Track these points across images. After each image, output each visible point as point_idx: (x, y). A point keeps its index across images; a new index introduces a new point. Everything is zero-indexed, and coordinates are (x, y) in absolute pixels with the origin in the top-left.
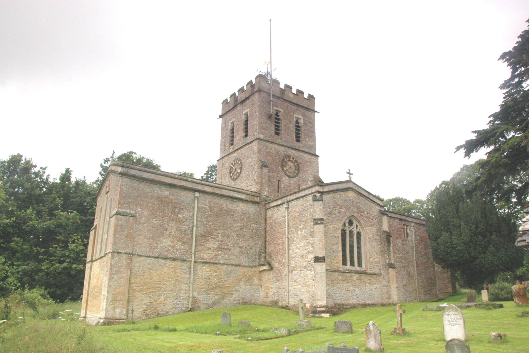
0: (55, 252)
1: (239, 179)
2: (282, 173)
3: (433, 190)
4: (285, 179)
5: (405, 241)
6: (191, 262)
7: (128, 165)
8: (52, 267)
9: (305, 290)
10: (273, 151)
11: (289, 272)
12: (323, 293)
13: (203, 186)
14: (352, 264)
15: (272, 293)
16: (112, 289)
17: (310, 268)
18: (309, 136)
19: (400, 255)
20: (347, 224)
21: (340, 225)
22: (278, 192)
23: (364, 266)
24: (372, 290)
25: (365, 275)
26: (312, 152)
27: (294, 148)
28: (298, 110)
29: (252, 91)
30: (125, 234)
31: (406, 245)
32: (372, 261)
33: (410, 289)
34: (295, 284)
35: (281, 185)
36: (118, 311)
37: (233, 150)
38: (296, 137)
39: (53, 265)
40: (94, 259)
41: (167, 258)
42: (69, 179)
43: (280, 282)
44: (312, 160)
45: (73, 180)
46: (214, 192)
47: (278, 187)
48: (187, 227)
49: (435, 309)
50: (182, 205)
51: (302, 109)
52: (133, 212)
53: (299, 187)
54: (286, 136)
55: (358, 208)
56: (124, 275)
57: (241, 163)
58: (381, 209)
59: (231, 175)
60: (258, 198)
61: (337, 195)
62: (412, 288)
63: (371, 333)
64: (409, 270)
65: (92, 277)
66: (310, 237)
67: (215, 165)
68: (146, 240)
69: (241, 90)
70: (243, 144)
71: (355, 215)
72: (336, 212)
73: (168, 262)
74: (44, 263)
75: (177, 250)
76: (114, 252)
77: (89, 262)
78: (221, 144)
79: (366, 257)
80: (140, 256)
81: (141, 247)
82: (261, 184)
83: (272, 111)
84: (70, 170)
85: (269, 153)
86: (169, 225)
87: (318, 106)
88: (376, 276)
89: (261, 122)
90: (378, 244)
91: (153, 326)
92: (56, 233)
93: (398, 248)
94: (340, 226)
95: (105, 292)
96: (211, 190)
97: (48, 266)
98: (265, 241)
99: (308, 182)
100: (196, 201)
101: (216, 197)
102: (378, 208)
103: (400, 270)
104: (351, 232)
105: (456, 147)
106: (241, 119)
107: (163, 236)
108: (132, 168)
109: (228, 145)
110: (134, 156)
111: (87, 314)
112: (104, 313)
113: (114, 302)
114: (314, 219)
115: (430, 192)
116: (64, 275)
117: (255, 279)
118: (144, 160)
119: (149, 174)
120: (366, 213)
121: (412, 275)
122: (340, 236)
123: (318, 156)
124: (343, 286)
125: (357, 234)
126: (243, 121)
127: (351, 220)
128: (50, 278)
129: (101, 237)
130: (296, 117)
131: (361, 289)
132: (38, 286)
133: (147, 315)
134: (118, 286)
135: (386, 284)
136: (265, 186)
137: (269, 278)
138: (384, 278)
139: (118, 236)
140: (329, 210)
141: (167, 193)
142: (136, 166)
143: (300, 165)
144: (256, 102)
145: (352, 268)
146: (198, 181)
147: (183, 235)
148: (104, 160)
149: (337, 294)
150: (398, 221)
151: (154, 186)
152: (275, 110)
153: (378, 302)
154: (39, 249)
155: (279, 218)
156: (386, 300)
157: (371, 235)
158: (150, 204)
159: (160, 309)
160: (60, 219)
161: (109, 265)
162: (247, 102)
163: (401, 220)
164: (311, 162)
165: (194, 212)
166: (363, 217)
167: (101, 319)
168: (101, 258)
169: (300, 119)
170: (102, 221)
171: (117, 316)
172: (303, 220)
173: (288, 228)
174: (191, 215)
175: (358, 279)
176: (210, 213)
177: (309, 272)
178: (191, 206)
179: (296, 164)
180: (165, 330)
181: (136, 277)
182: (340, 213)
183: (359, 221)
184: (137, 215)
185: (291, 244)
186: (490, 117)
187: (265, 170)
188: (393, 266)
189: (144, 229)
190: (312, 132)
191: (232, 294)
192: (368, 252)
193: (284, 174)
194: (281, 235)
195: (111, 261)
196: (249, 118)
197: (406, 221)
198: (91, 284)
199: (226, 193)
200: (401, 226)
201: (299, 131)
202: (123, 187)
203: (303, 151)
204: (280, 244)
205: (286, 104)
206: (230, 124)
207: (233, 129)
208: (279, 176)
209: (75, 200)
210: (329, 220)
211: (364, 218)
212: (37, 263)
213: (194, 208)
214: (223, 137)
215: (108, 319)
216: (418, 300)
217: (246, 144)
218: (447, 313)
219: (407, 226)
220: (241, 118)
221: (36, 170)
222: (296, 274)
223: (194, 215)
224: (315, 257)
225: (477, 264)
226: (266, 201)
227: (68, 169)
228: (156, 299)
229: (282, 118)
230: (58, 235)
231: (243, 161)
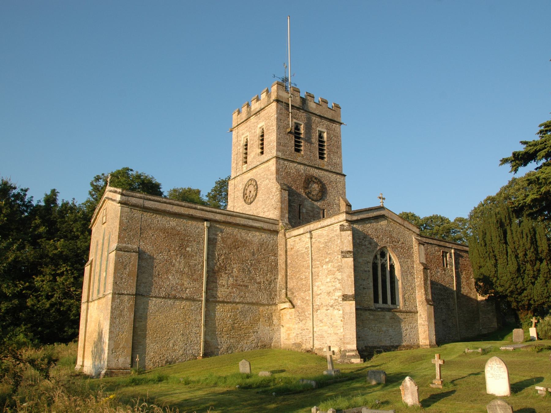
3: (476, 206)
6: (202, 301)
9: (332, 332)
11: (313, 311)
12: (353, 335)
14: (385, 301)
15: (295, 334)
17: (337, 307)
20: (379, 256)
21: (371, 258)
26: (338, 171)
34: (321, 325)
35: (302, 210)
37: (247, 169)
38: (320, 153)
43: (304, 322)
45: (59, 203)
46: (226, 220)
48: (196, 262)
63: (408, 389)
65: (88, 320)
66: (338, 272)
67: (224, 180)
94: (371, 258)
98: (286, 275)
103: (439, 304)
105: (502, 159)
106: (256, 134)
108: (133, 197)
109: (241, 163)
110: (130, 173)
114: (342, 252)
115: (473, 209)
117: (275, 318)
119: (152, 202)
122: (371, 270)
123: (345, 176)
124: (374, 327)
126: (258, 136)
129: (98, 275)
130: (319, 131)
131: (394, 329)
135: (423, 323)
136: (285, 212)
137: (291, 317)
140: (358, 241)
144: (273, 115)
145: (385, 306)
149: (368, 335)
152: (295, 123)
155: (300, 249)
156: (423, 341)
161: (110, 308)
162: (263, 113)
163: (439, 246)
170: (99, 256)
172: (329, 252)
173: (312, 262)
175: (392, 318)
177: (336, 312)
181: (141, 320)
185: (316, 279)
186: (540, 126)
189: (148, 266)
190: (338, 148)
191: (249, 337)
194: (304, 269)
199: (240, 221)
201: (322, 147)
203: (327, 171)
204: (303, 279)
207: (246, 145)
208: (301, 199)
218: (490, 365)
221: (15, 192)
222: (320, 314)
224: (343, 296)
227: (54, 190)
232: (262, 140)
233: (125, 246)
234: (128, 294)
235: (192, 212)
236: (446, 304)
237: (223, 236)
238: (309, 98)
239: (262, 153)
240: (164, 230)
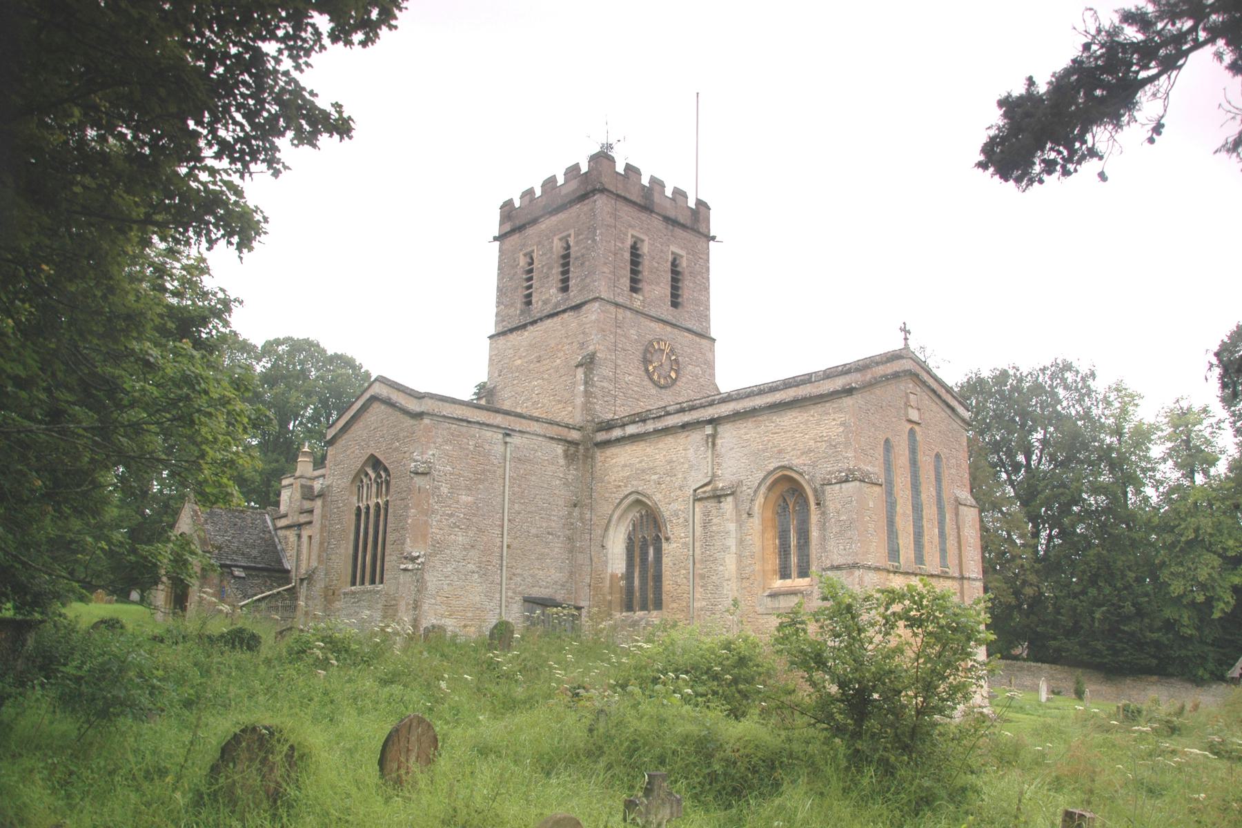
130: (673, 253)
146: (459, 412)
169: (682, 257)
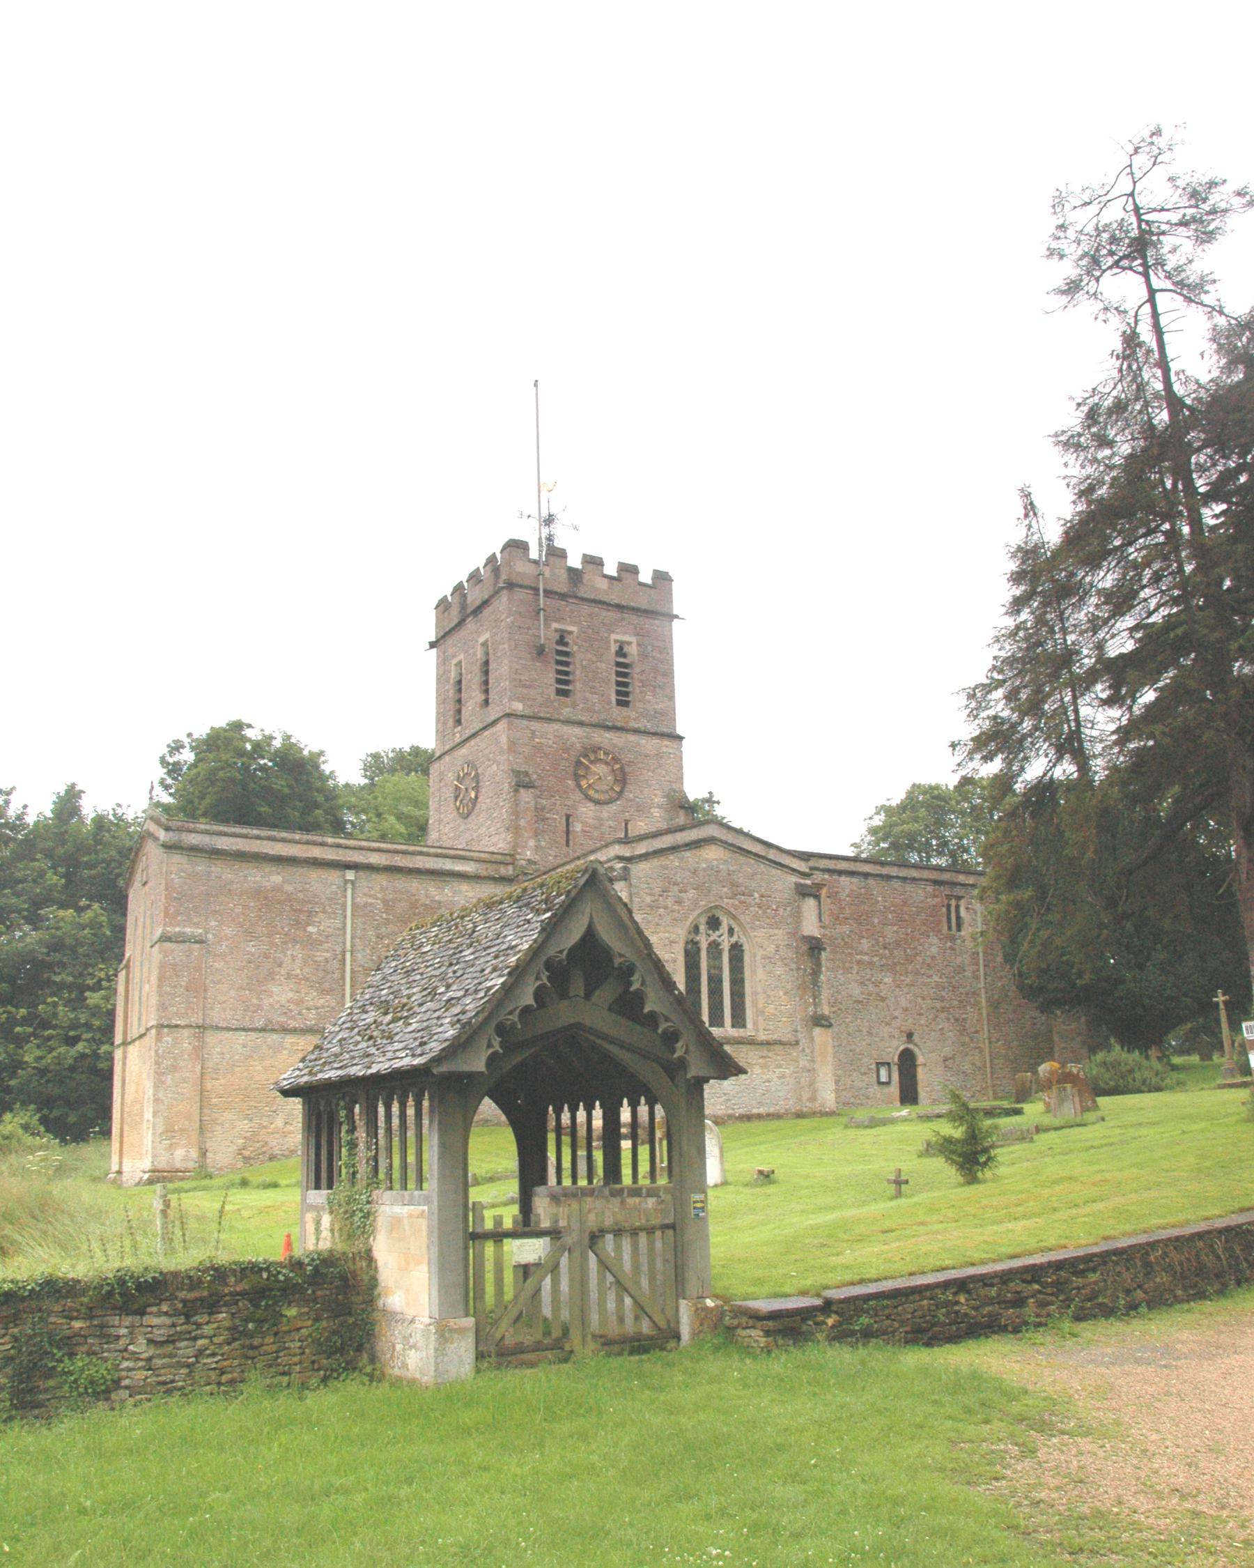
0: (55, 1015)
1: (473, 816)
2: (578, 796)
4: (587, 811)
5: (953, 939)
7: (180, 823)
8: (50, 1056)
10: (551, 742)
13: (364, 852)
16: (161, 1107)
18: (655, 687)
19: (936, 978)
20: (702, 928)
21: (680, 932)
22: (568, 845)
23: (749, 1024)
24: (769, 1082)
25: (748, 1046)
26: (666, 730)
27: (610, 724)
28: (623, 619)
29: (495, 585)
30: (183, 984)
31: (954, 949)
32: (772, 1011)
33: (967, 1067)
36: (179, 1153)
39: (51, 1049)
40: (129, 1040)
41: (286, 1030)
42: (75, 811)
44: (664, 749)
47: (568, 832)
49: (866, 1123)
50: (316, 903)
51: (634, 617)
52: (200, 931)
53: (626, 824)
54: (588, 694)
55: (733, 885)
56: (188, 1074)
57: (477, 775)
58: (802, 881)
59: (458, 803)
60: (510, 868)
61: (673, 860)
62: (973, 1064)
64: (964, 1016)
65: (127, 1079)
68: (233, 993)
69: (475, 577)
70: (481, 726)
71: (725, 902)
72: (670, 902)
73: (289, 1039)
74: (30, 1045)
75: (308, 1009)
76: (162, 1026)
77: (119, 1046)
78: (438, 721)
79: (755, 1003)
80: (223, 1029)
81: (224, 1010)
82: (515, 829)
83: (546, 634)
84: (78, 788)
85: (538, 749)
86: (285, 955)
87: (680, 602)
88: (782, 1047)
89: (517, 670)
90: (792, 970)
91: (237, 1178)
92: (49, 966)
93: (928, 960)
95: (148, 1115)
96: (387, 859)
97: (38, 1053)
99: (652, 810)
100: (349, 892)
101: (399, 876)
102: (794, 879)
104: (714, 947)
107: (273, 979)
109: (451, 723)
110: (248, 733)
111: (124, 1164)
112: (150, 1160)
113: (169, 1134)
116: (82, 1073)
118: (277, 743)
119: (232, 840)
120: (756, 895)
121: (973, 1030)
123: (681, 738)
125: (730, 951)
126: (478, 664)
127: (714, 916)
128: (48, 1081)
130: (616, 641)
132: (18, 1105)
133: (247, 1159)
134: (175, 1099)
136: (526, 835)
138: (803, 1050)
139: (168, 989)
141: (276, 879)
142: (198, 825)
143: (628, 769)
147: (321, 974)
148: (169, 746)
150: (930, 889)
151: (244, 865)
152: (556, 630)
153: (786, 1110)
154: (13, 1010)
157: (772, 948)
158: (239, 910)
159: (275, 1144)
160: (58, 929)
161: (153, 1054)
162: (487, 611)
163: (937, 883)
164: (662, 757)
165: (345, 917)
166: (748, 906)
167: (145, 1172)
168: (141, 1036)
169: (629, 643)
170: (138, 951)
171: (178, 1165)
174: (339, 926)
176: (384, 916)
178: (338, 904)
179: (617, 766)
180: (258, 1187)
181: (215, 1076)
182: (679, 902)
183: (734, 917)
184: (210, 936)
187: (526, 796)
188: (826, 1020)
192: (759, 990)
193: (583, 796)
195: (156, 1045)
196: (492, 657)
197: (954, 884)
198: (126, 1096)
200: (939, 899)
202: (173, 876)
205: (586, 609)
206: (453, 668)
207: (460, 682)
209: (93, 872)
210: (649, 922)
211: (752, 909)
212: (12, 1046)
213: (344, 907)
214: (441, 701)
215: (158, 1171)
216: (991, 1093)
217: (485, 724)
219: (959, 898)
220: (475, 654)
223: (344, 924)
225: (1121, 998)
226: (526, 874)
228: (265, 1124)
229: (575, 648)
230: (57, 970)
231: (480, 771)
232: (486, 673)
233: (179, 932)
234: (187, 1026)
235: (317, 852)
236: (957, 1020)
237: (387, 898)
238: (590, 567)
239: (486, 702)
240: (257, 893)
